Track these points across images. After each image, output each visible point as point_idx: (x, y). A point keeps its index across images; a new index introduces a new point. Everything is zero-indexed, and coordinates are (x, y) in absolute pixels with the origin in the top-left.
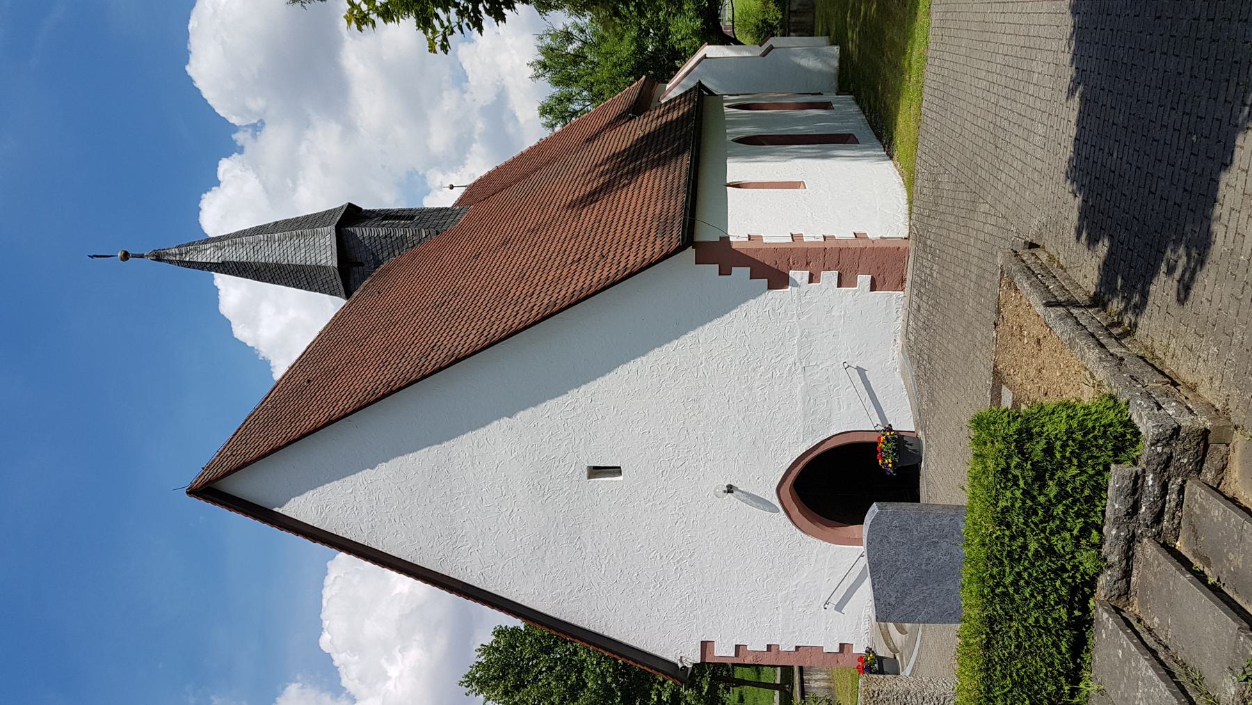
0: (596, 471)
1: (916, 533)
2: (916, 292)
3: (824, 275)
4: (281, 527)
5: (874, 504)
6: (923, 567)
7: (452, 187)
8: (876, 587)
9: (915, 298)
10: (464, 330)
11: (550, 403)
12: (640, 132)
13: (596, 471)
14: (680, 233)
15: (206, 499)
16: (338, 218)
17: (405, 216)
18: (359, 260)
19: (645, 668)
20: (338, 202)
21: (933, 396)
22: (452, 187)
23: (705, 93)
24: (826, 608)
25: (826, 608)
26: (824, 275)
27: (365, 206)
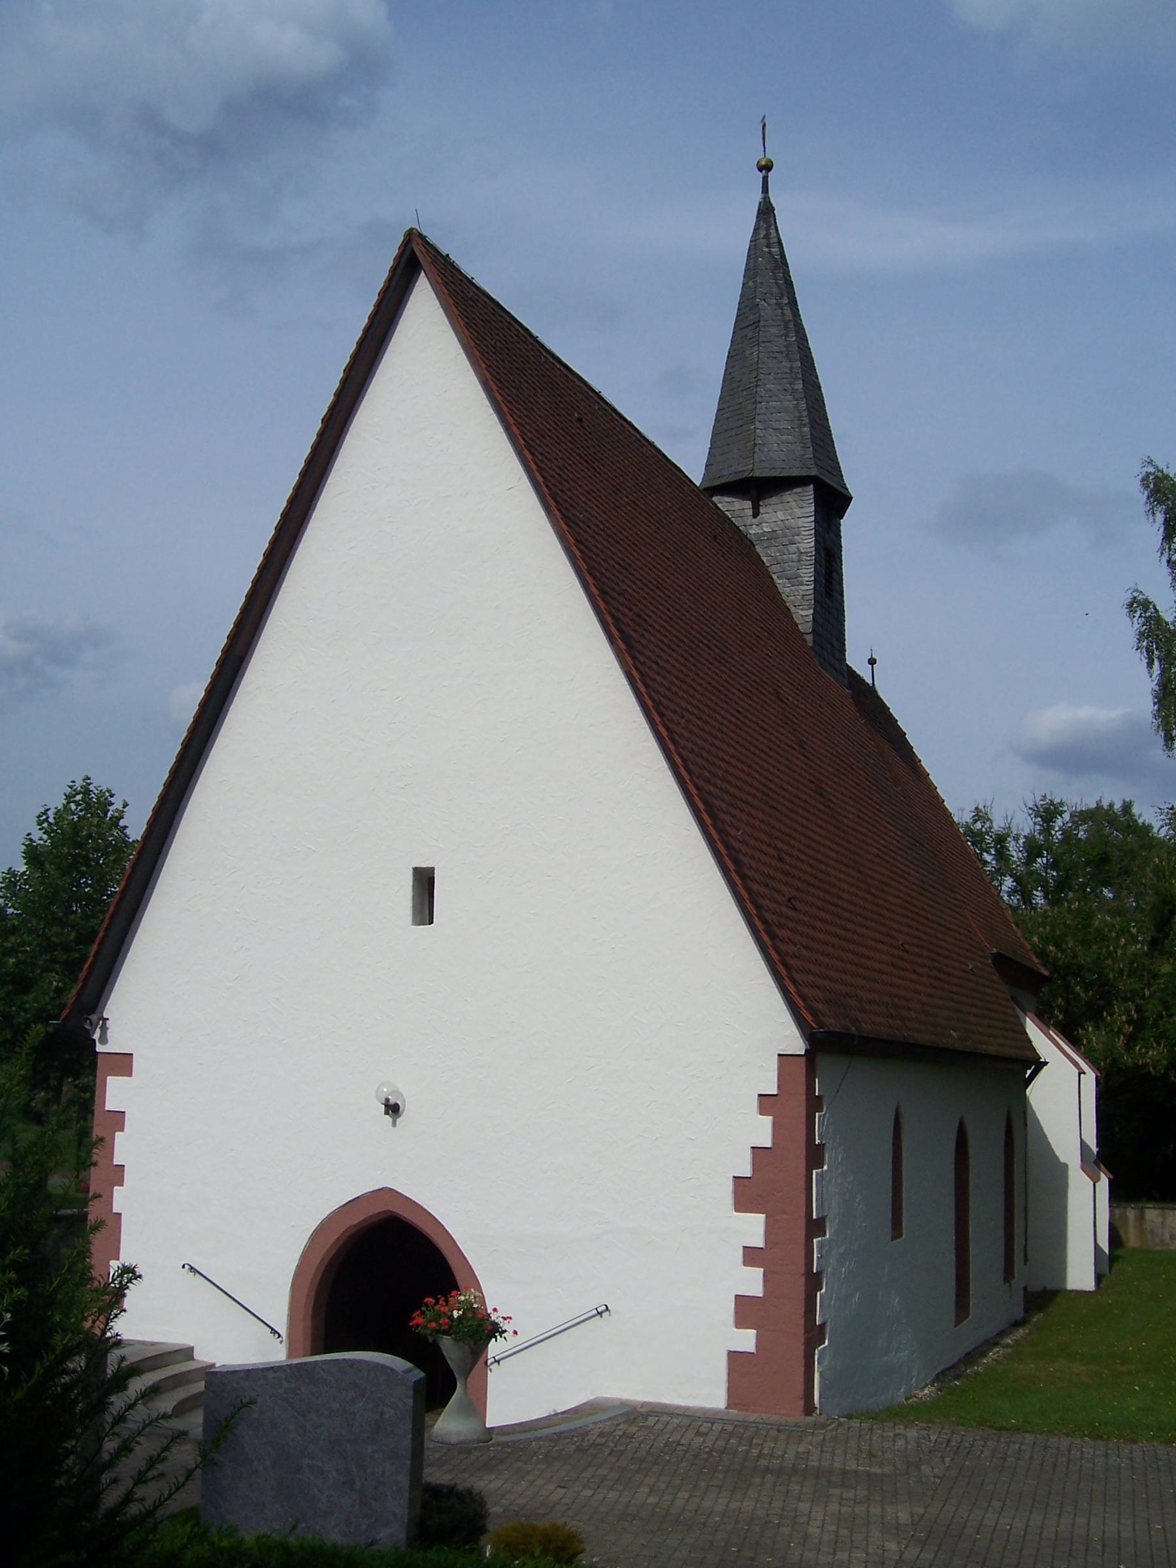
0: (424, 881)
1: (369, 1450)
2: (730, 1428)
3: (758, 1273)
4: (350, 370)
5: (422, 1374)
6: (306, 1461)
7: (872, 662)
8: (271, 1375)
9: (717, 1427)
10: (669, 667)
11: (129, 955)
12: (971, 967)
13: (424, 881)
14: (832, 1029)
15: (398, 259)
16: (828, 481)
17: (831, 583)
18: (762, 510)
19: (91, 959)
20: (852, 481)
21: (555, 1459)
22: (872, 662)
23: (1029, 1072)
24: (183, 1267)
25: (183, 1267)
26: (758, 1273)
27: (848, 524)
